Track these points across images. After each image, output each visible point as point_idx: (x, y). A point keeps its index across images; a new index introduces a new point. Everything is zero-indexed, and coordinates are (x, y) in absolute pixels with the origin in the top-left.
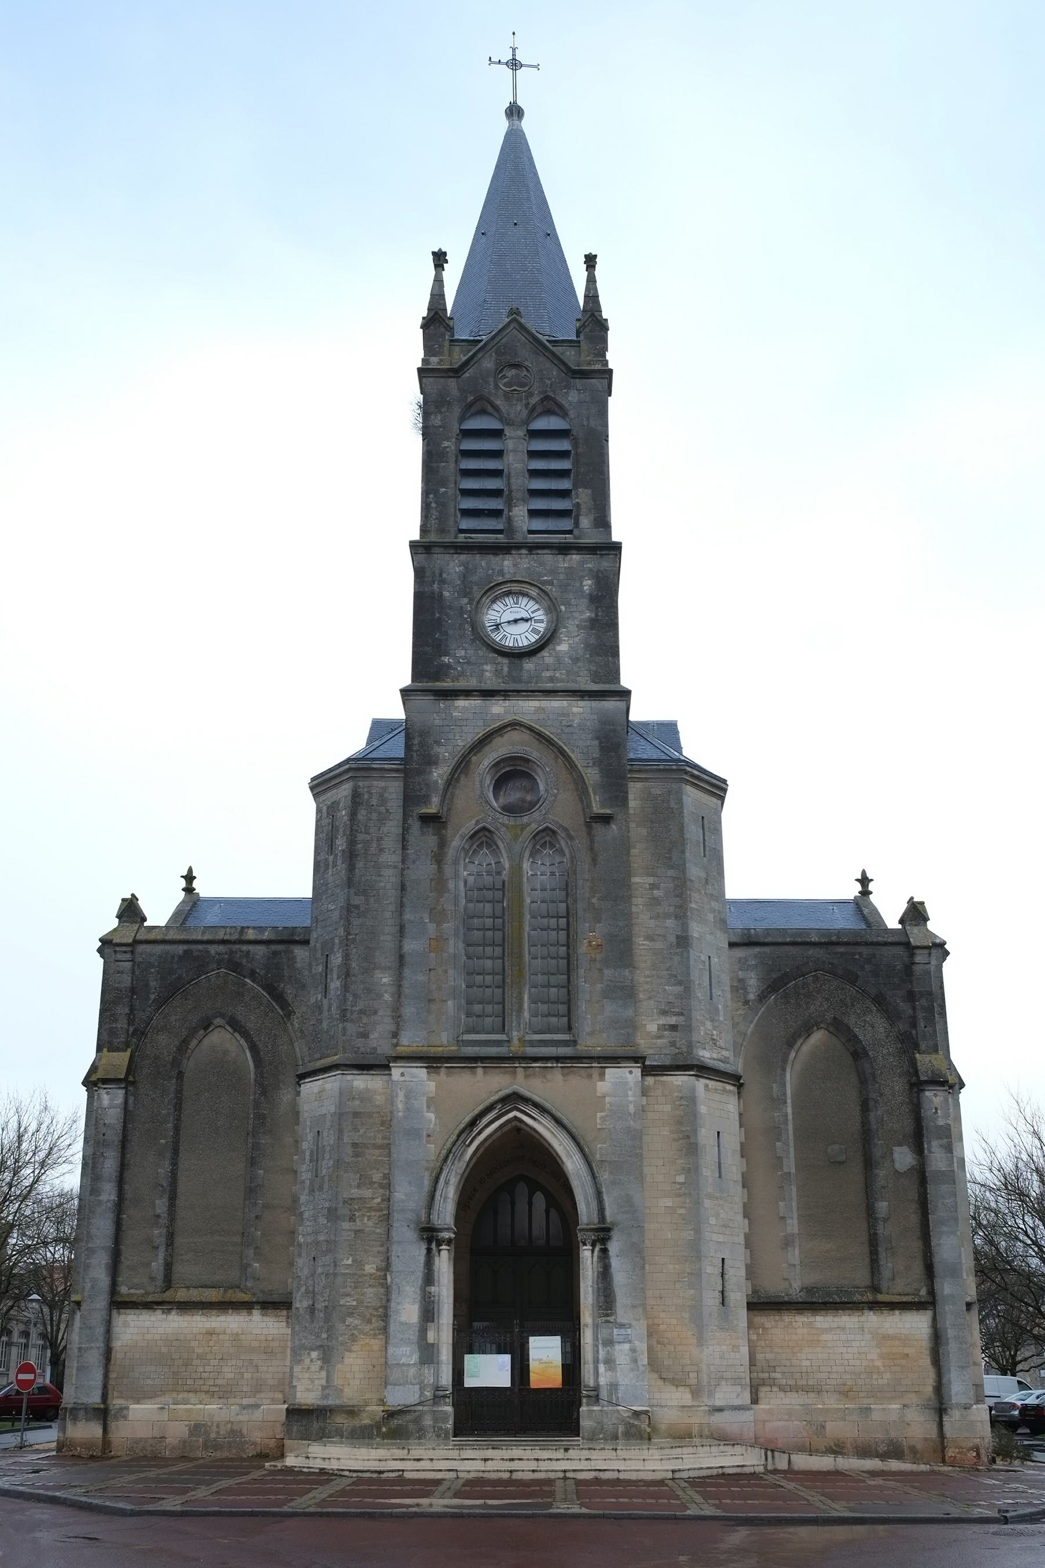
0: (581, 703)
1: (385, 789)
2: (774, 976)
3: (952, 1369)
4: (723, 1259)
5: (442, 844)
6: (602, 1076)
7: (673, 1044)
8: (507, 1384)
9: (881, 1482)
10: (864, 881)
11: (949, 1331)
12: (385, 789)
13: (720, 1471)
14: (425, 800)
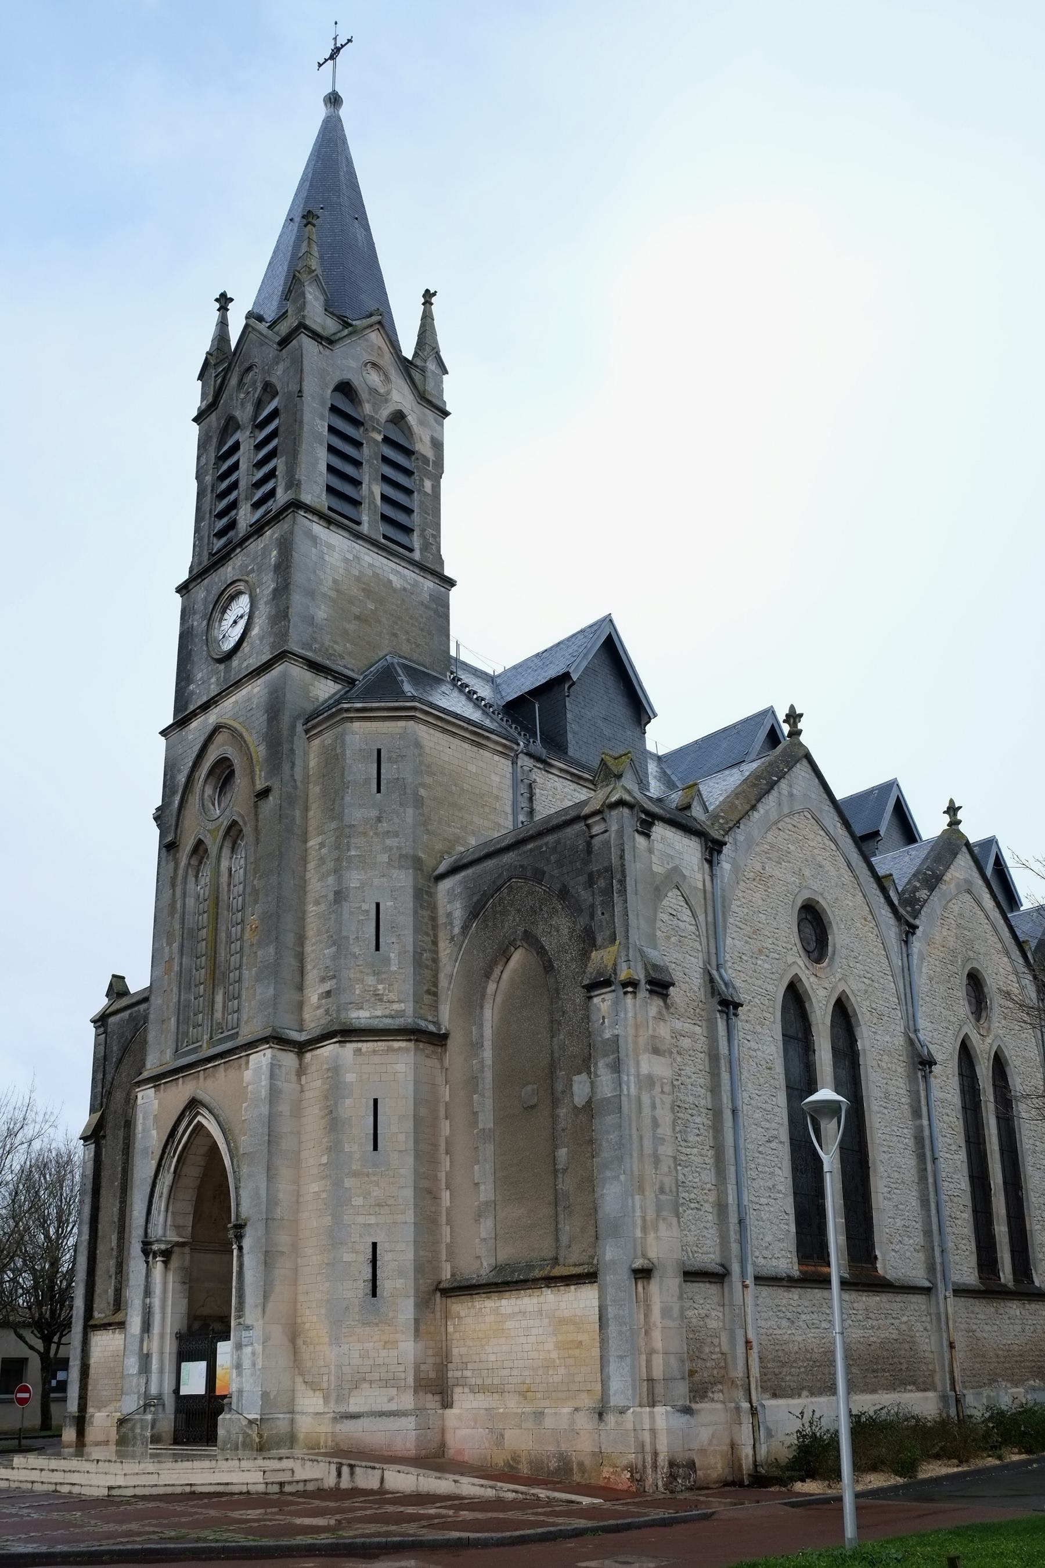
2: (475, 899)
3: (612, 1359)
4: (374, 1245)
7: (327, 1011)
8: (203, 1392)
9: (230, 1514)
11: (610, 1309)
13: (188, 1489)
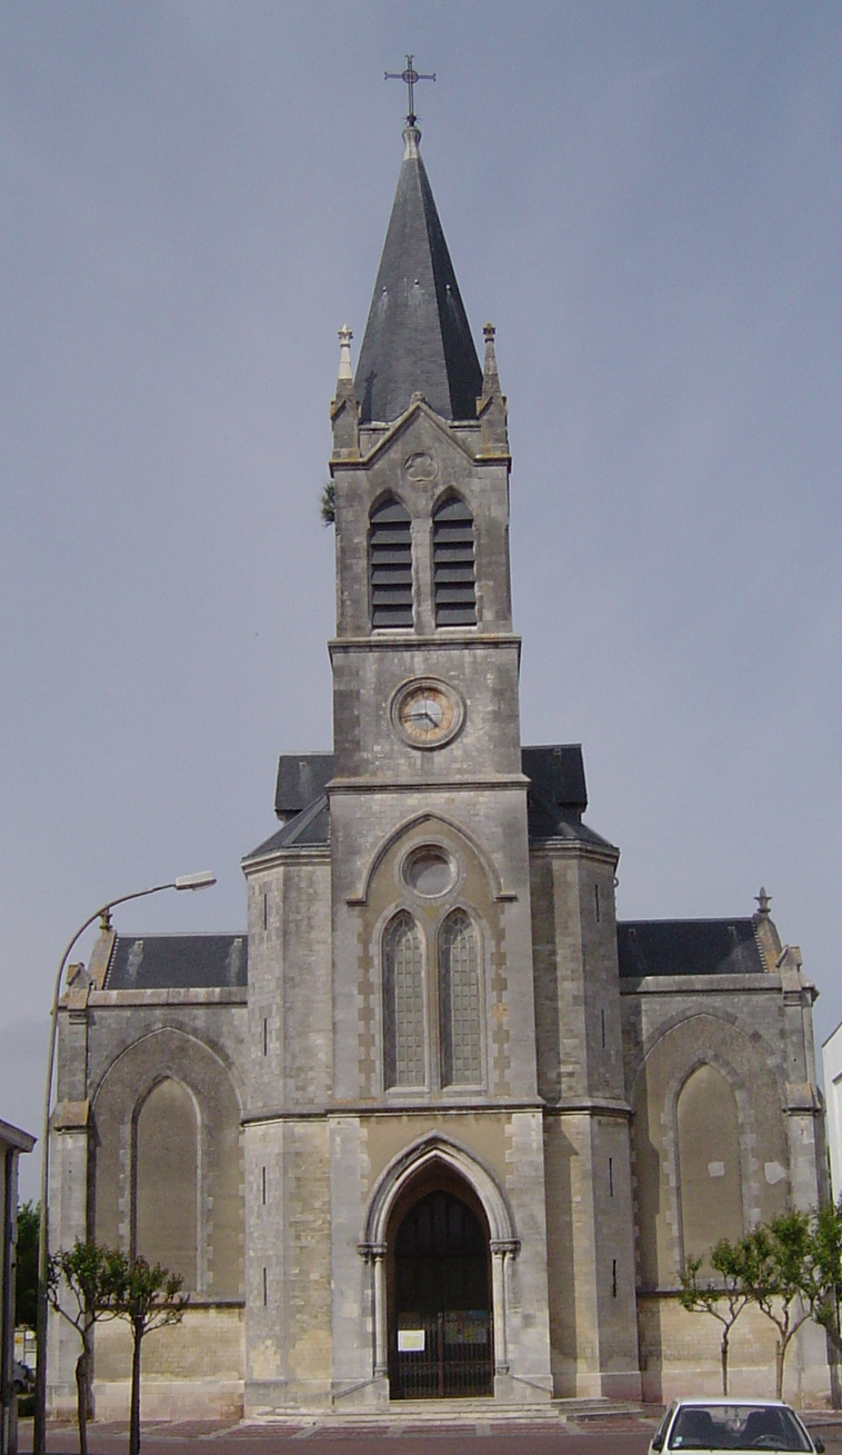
0: (486, 793)
1: (313, 872)
5: (368, 926)
6: (509, 1119)
10: (763, 899)
12: (313, 872)
14: (351, 886)
